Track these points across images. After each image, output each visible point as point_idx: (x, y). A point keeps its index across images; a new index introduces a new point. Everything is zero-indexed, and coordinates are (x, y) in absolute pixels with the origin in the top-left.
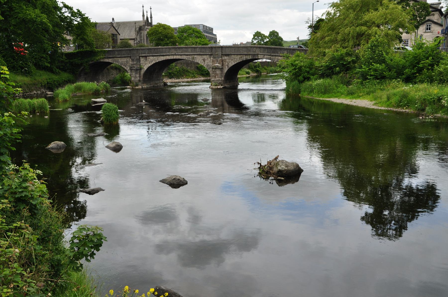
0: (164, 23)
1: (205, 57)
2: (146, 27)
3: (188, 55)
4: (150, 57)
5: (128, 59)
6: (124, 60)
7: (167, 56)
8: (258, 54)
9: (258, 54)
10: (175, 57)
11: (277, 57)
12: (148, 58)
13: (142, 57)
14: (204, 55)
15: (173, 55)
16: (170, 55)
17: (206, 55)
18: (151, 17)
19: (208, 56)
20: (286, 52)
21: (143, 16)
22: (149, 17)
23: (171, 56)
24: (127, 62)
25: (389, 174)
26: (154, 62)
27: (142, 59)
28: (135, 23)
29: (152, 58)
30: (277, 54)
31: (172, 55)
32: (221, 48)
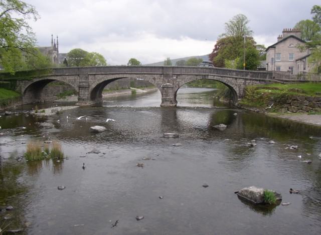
0: (86, 50)
1: (155, 76)
2: (54, 51)
3: (138, 74)
4: (99, 76)
5: (76, 77)
6: (72, 78)
7: (117, 75)
8: (208, 75)
9: (208, 75)
10: (117, 76)
11: (226, 78)
12: (96, 76)
13: (90, 75)
14: (154, 74)
15: (123, 74)
16: (119, 74)
17: (157, 74)
18: (58, 44)
19: (158, 75)
20: (234, 74)
21: (52, 43)
22: (56, 43)
23: (121, 75)
24: (75, 80)
25: (19, 202)
26: (103, 80)
27: (90, 77)
28: (46, 48)
29: (101, 76)
30: (226, 76)
31: (122, 74)
32: (172, 69)
